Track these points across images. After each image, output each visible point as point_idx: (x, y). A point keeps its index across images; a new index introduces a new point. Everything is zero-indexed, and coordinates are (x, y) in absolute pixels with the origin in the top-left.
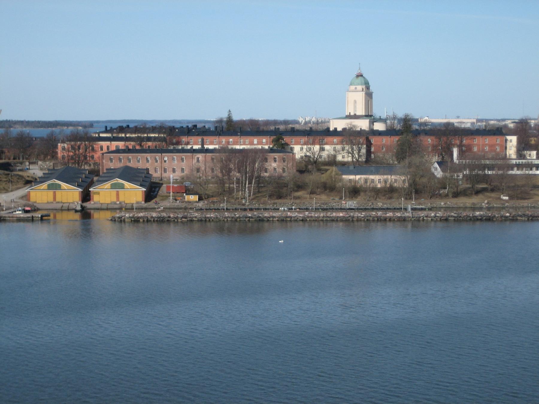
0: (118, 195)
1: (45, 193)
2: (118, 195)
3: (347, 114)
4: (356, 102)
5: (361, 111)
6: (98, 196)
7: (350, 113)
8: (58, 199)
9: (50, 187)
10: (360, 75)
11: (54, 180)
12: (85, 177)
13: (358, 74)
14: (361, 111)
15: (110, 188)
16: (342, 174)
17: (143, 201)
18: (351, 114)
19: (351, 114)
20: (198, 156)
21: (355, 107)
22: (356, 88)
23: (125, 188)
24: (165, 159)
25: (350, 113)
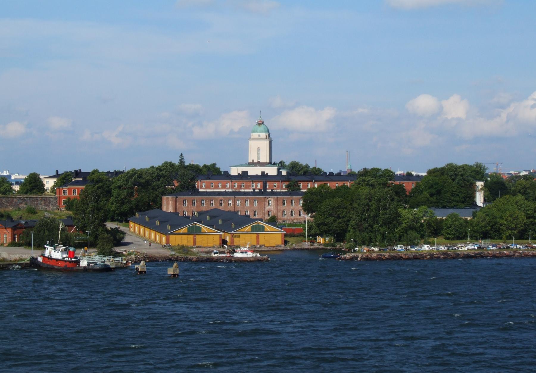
0: (258, 238)
1: (248, 237)
2: (258, 238)
3: (250, 161)
4: (259, 150)
5: (265, 159)
6: (238, 239)
7: (253, 160)
8: (262, 242)
9: (254, 229)
10: (260, 123)
11: (195, 222)
12: (211, 218)
13: (259, 121)
14: (265, 159)
15: (250, 231)
16: (104, 223)
17: (282, 244)
18: (254, 162)
19: (254, 162)
20: (269, 199)
21: (259, 155)
22: (259, 136)
23: (265, 231)
24: (229, 202)
25: (253, 160)
